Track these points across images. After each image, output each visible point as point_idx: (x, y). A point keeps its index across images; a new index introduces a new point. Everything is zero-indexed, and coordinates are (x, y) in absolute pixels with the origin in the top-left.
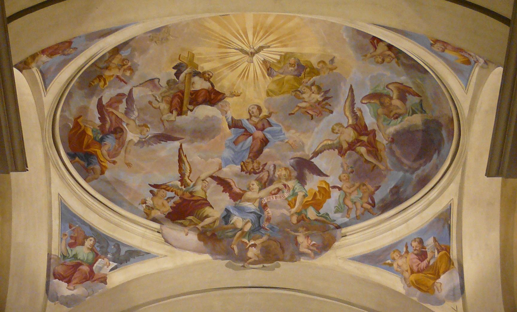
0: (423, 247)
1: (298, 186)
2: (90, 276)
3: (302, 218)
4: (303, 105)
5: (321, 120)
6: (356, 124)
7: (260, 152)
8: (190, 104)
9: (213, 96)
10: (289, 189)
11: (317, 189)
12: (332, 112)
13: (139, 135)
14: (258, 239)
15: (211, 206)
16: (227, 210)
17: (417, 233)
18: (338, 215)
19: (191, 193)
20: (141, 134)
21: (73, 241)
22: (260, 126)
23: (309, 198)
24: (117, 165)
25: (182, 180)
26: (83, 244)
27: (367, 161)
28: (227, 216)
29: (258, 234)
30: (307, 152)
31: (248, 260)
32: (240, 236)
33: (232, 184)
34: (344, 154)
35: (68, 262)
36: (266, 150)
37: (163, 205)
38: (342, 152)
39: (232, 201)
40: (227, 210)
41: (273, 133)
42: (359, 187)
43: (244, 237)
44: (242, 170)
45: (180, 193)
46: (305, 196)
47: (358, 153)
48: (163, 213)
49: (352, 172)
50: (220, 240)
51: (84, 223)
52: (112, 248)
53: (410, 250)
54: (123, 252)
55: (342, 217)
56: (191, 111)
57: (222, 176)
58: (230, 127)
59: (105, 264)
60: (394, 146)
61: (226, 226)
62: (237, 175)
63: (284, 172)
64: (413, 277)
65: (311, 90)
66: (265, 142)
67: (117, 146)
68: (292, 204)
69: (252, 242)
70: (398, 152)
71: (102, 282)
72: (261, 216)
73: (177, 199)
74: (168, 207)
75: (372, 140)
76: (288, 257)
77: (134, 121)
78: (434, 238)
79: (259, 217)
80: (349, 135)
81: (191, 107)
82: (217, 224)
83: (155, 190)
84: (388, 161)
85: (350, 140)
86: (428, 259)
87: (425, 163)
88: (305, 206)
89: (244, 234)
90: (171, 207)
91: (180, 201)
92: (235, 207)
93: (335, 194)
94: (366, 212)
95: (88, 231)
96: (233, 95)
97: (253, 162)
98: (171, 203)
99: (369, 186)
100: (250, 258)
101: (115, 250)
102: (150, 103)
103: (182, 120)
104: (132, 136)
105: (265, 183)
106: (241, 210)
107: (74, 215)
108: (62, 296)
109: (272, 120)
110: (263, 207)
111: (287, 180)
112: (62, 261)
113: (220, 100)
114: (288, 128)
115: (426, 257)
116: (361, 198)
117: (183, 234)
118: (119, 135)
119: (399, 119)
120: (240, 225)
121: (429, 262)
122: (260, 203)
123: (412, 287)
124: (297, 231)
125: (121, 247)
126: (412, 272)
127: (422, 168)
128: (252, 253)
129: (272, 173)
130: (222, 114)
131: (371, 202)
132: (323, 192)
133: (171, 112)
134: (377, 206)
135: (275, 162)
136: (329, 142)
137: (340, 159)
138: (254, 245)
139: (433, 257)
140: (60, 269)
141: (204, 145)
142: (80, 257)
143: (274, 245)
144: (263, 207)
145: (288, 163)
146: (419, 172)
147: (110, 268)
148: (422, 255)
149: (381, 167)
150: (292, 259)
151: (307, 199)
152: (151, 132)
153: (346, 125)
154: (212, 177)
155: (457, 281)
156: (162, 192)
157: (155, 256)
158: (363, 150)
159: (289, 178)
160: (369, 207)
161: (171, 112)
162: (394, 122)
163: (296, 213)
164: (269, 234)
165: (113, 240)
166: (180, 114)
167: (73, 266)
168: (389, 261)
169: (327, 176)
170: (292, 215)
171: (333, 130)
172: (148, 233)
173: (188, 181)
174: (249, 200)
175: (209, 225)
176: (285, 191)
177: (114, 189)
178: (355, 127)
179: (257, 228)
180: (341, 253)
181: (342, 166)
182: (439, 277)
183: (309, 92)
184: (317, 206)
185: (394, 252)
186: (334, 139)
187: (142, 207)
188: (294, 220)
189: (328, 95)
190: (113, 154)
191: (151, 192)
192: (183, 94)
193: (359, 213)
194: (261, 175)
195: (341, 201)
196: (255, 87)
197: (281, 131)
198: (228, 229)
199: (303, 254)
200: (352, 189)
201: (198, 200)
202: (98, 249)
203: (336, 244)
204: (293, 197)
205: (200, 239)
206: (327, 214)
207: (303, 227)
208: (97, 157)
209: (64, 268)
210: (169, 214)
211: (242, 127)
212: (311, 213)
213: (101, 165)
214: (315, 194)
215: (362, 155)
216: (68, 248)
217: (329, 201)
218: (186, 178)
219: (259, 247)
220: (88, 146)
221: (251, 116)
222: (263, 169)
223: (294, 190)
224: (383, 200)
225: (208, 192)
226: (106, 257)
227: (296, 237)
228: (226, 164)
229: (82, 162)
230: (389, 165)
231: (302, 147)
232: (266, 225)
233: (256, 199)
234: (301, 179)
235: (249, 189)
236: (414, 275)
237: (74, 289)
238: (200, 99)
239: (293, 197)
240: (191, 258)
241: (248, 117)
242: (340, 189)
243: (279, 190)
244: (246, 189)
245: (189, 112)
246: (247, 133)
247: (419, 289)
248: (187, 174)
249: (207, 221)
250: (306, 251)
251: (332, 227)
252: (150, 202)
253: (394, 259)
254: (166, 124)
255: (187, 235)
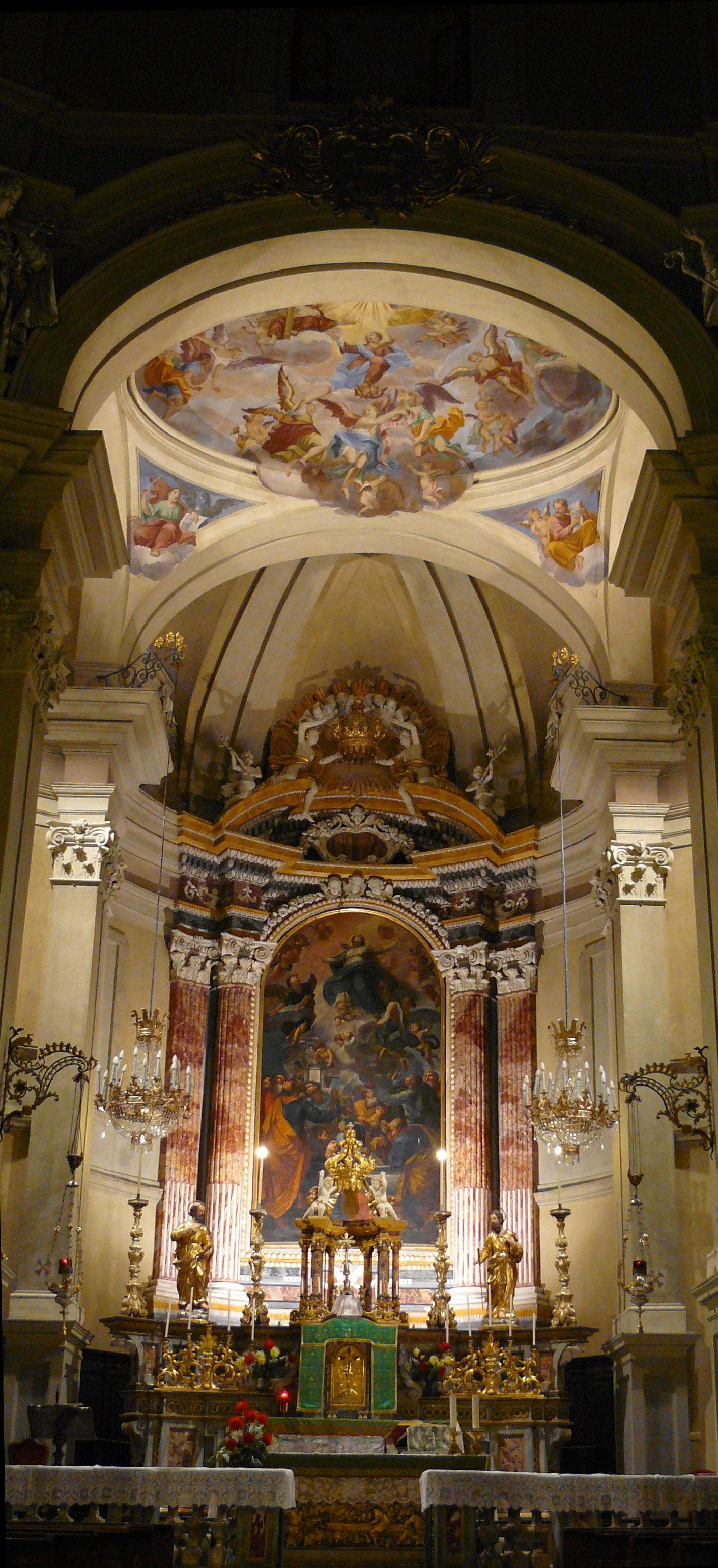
0: (567, 511)
1: (424, 413)
2: (177, 537)
3: (428, 448)
4: (434, 334)
5: (454, 349)
6: (499, 355)
7: (379, 376)
8: (293, 329)
9: (321, 323)
10: (414, 416)
11: (448, 417)
12: (469, 342)
13: (230, 359)
14: (373, 479)
15: (317, 432)
16: (337, 437)
17: (561, 494)
18: (472, 447)
19: (293, 417)
20: (232, 357)
21: (155, 496)
22: (379, 351)
23: (438, 426)
24: (202, 391)
25: (283, 403)
26: (166, 498)
27: (509, 391)
28: (337, 446)
29: (373, 473)
30: (437, 377)
31: (361, 508)
32: (352, 476)
33: (344, 408)
34: (483, 382)
35: (150, 521)
36: (386, 375)
37: (259, 431)
38: (479, 379)
39: (343, 426)
40: (337, 437)
41: (395, 359)
42: (499, 417)
43: (357, 477)
44: (357, 394)
45: (280, 417)
46: (433, 423)
47: (499, 382)
48: (260, 442)
49: (491, 401)
50: (329, 481)
51: (166, 473)
52: (201, 498)
53: (552, 511)
54: (213, 503)
55: (477, 450)
56: (295, 335)
57: (331, 399)
58: (342, 352)
59: (194, 519)
60: (543, 381)
61: (335, 460)
62: (350, 399)
63: (407, 398)
64: (552, 545)
65: (444, 321)
66: (385, 367)
67: (203, 371)
68: (416, 432)
69: (367, 484)
70: (548, 388)
71: (190, 543)
72: (378, 446)
73: (276, 424)
74: (265, 436)
75: (517, 372)
76: (408, 506)
77: (224, 346)
78: (581, 503)
79: (376, 447)
80: (490, 364)
81: (295, 332)
82: (325, 455)
83: (249, 415)
84: (536, 394)
85: (490, 369)
86: (571, 525)
87: (579, 405)
88: (433, 434)
89: (358, 473)
90: (269, 434)
91: (280, 426)
92: (347, 434)
93: (470, 423)
94: (506, 449)
95: (171, 481)
96: (346, 322)
97: (370, 387)
98: (269, 429)
99: (512, 418)
100: (364, 506)
101: (204, 501)
102: (244, 328)
103: (281, 344)
104: (220, 360)
105: (384, 408)
106: (354, 438)
107: (156, 467)
108: (146, 565)
109: (395, 346)
110: (381, 435)
111: (411, 406)
112: (144, 522)
113: (331, 327)
114: (414, 354)
115: (570, 523)
116: (501, 430)
117: (284, 475)
118: (205, 360)
119: (551, 357)
120: (352, 458)
121: (572, 529)
122: (378, 430)
123: (550, 559)
124: (420, 469)
125: (211, 497)
126: (552, 539)
127: (575, 410)
128: (366, 498)
129: (393, 397)
130: (333, 339)
131: (511, 435)
132: (455, 420)
133: (270, 336)
134: (518, 442)
135: (398, 387)
136: (465, 369)
137: (477, 387)
138: (369, 488)
139: (578, 524)
140: (141, 532)
141: (310, 368)
142: (164, 513)
143: (393, 489)
144: (381, 435)
145: (414, 388)
146: (572, 412)
147: (199, 524)
148: (565, 520)
149: (527, 398)
150: (413, 509)
151: (434, 427)
152: (245, 355)
153: (485, 354)
154: (320, 400)
155: (602, 559)
156: (258, 417)
157: (252, 505)
158: (506, 380)
159: (414, 404)
160: (510, 442)
161: (270, 336)
162: (543, 358)
163: (421, 443)
164: (386, 472)
165: (201, 489)
166: (281, 337)
167: (157, 525)
168: (526, 522)
169: (459, 402)
170: (416, 445)
171: (470, 358)
172: (244, 476)
173: (290, 404)
174: (364, 426)
175: (314, 457)
176: (409, 417)
177: (199, 419)
178: (496, 357)
179: (373, 464)
180: (472, 504)
181: (479, 393)
182: (581, 550)
183: (441, 324)
184: (447, 432)
185: (533, 511)
186: (471, 366)
187: (234, 438)
188: (418, 451)
189: (464, 327)
190: (198, 381)
191: (245, 417)
192: (285, 319)
193: (497, 447)
194: (380, 400)
195: (477, 429)
196: (374, 316)
197: (405, 357)
198: (336, 464)
199: (426, 502)
200: (491, 418)
201: (301, 425)
202: (184, 501)
203: (467, 492)
204: (418, 425)
205: (304, 480)
206: (459, 445)
207: (429, 462)
208: (179, 385)
209: (147, 529)
210: (267, 442)
211: (357, 352)
212: (439, 443)
213: (183, 394)
214: (445, 422)
215: (504, 384)
216: (150, 505)
217: (461, 430)
218: (288, 401)
219: (375, 490)
220: (168, 376)
221: (368, 343)
222: (382, 394)
223: (419, 417)
224: (526, 436)
225: (315, 416)
226: (194, 510)
227: (419, 478)
228: (337, 388)
229: (161, 395)
230: (536, 398)
231: (431, 372)
232: (383, 458)
233: (372, 426)
234: (429, 406)
235: (364, 414)
236: (553, 543)
237: (159, 554)
238: (306, 325)
239: (418, 425)
240: (294, 504)
241: (366, 343)
242: (475, 417)
243: (401, 416)
244: (360, 413)
245: (292, 337)
246: (363, 358)
247: (557, 561)
248: (289, 396)
249: (313, 452)
250: (430, 498)
251: (463, 463)
252: (243, 430)
253: (532, 520)
254: (263, 347)
255: (288, 475)
